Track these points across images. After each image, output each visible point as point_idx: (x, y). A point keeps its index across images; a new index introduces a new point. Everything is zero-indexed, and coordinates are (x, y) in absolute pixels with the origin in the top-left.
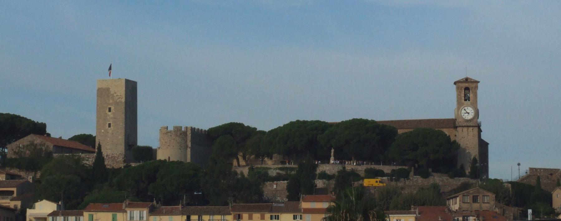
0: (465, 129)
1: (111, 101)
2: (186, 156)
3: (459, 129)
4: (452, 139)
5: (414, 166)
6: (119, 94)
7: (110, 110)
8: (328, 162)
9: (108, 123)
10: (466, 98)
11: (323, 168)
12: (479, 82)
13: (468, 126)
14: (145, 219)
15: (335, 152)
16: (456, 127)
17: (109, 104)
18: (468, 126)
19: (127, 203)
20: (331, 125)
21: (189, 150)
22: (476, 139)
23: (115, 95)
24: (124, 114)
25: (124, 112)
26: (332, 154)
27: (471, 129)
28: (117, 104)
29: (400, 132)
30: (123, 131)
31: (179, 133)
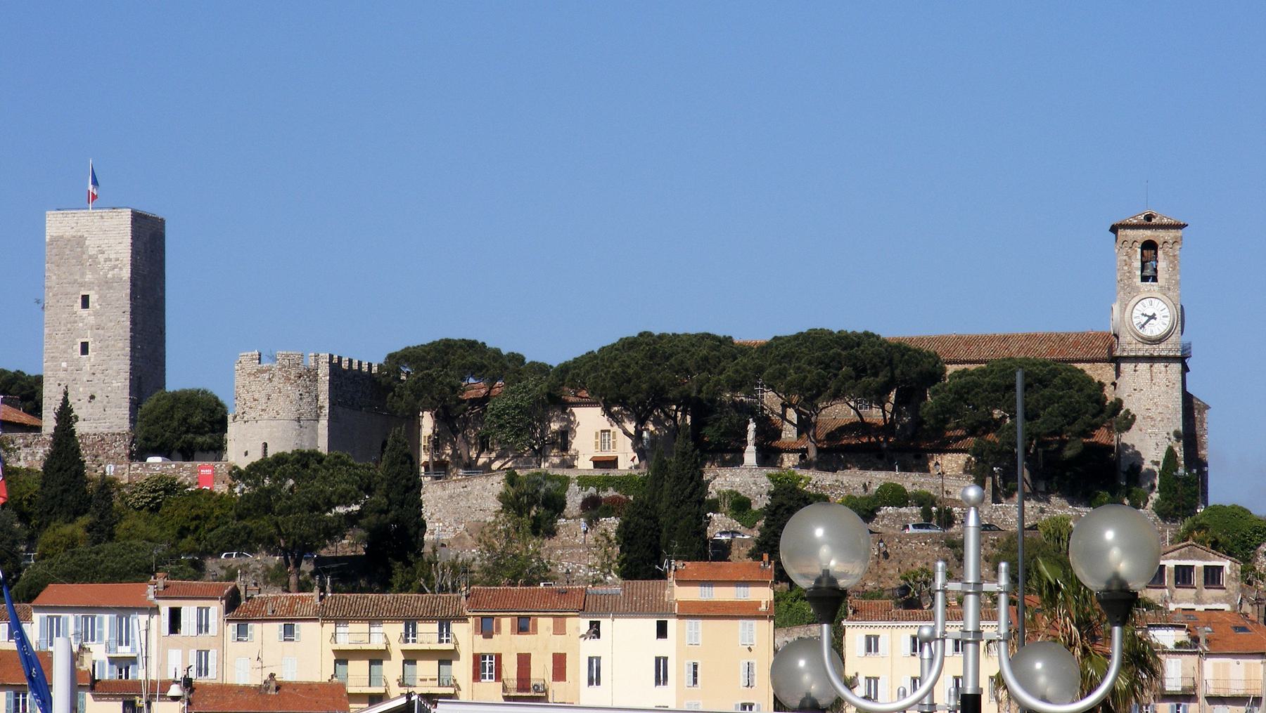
0: (1143, 367)
1: (89, 277)
2: (314, 439)
3: (1126, 367)
4: (1110, 395)
5: (993, 474)
6: (113, 256)
7: (85, 302)
8: (738, 461)
9: (79, 341)
10: (1148, 272)
11: (721, 480)
12: (1207, 407)
13: (1151, 359)
14: (213, 629)
15: (756, 430)
16: (1117, 361)
17: (82, 285)
18: (1151, 359)
19: (161, 583)
20: (744, 350)
21: (324, 423)
22: (1179, 394)
23: (101, 258)
24: (128, 315)
25: (128, 308)
26: (751, 436)
27: (1159, 366)
28: (106, 284)
29: (951, 369)
30: (125, 365)
31: (293, 372)
